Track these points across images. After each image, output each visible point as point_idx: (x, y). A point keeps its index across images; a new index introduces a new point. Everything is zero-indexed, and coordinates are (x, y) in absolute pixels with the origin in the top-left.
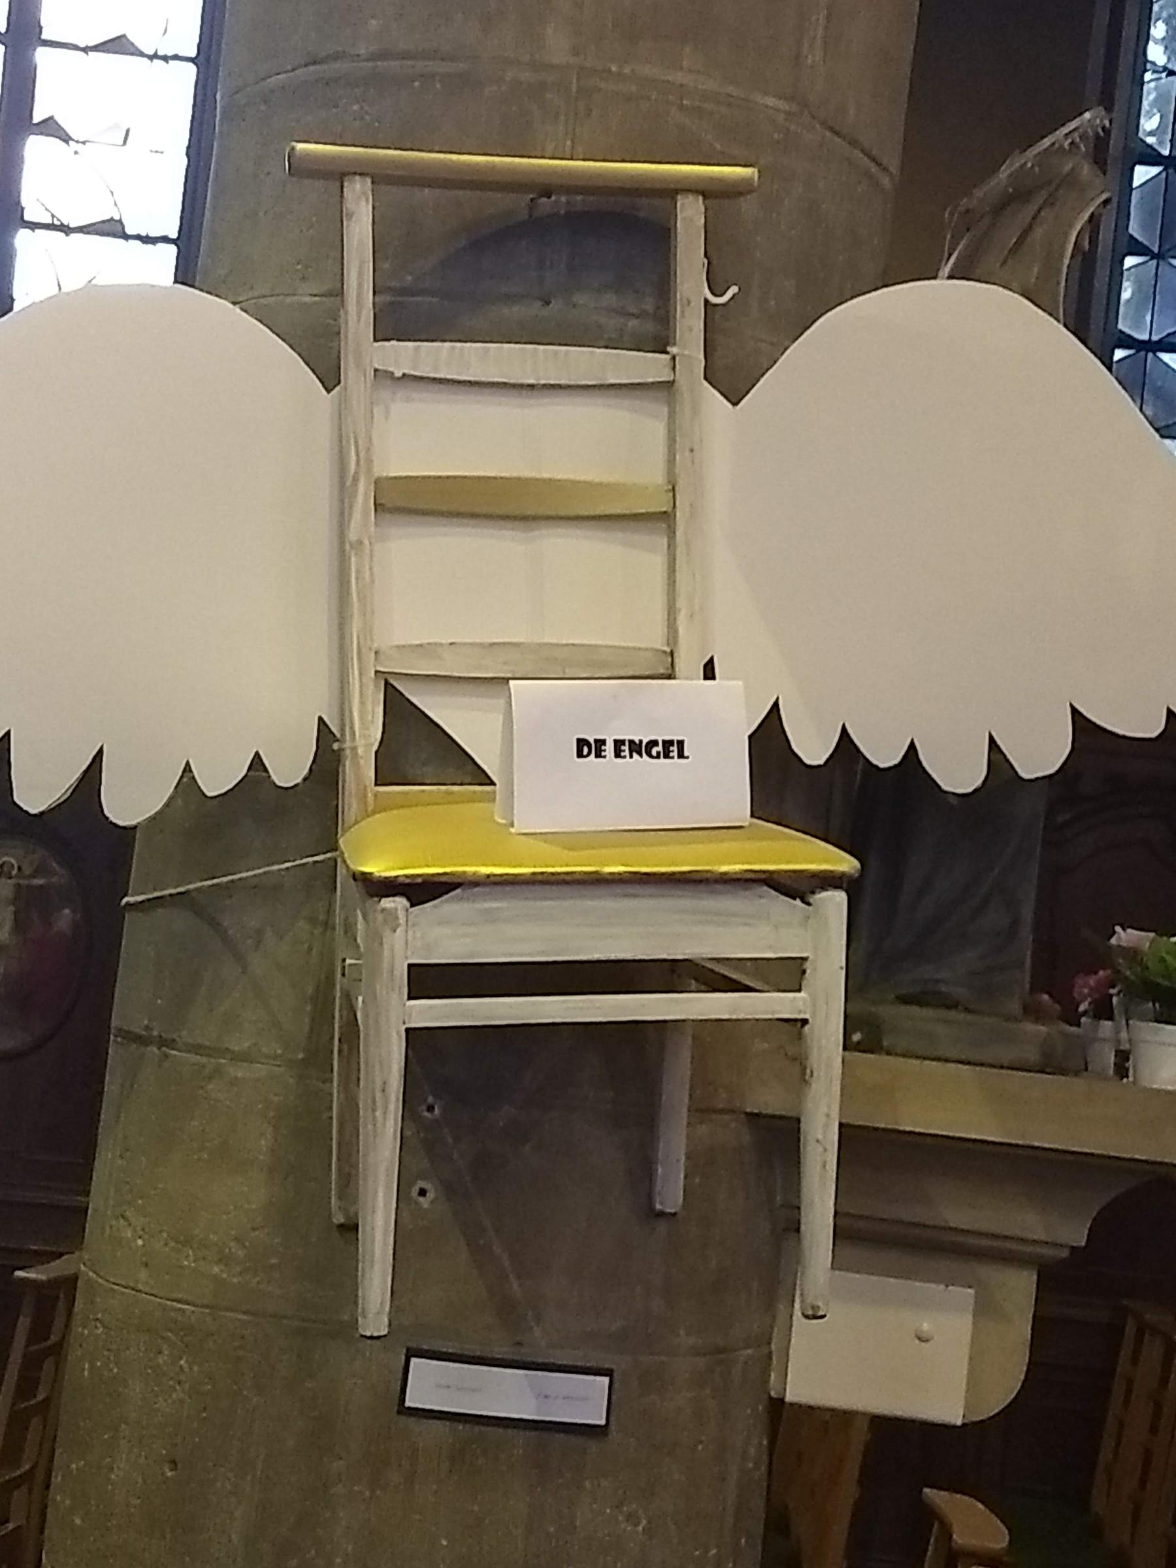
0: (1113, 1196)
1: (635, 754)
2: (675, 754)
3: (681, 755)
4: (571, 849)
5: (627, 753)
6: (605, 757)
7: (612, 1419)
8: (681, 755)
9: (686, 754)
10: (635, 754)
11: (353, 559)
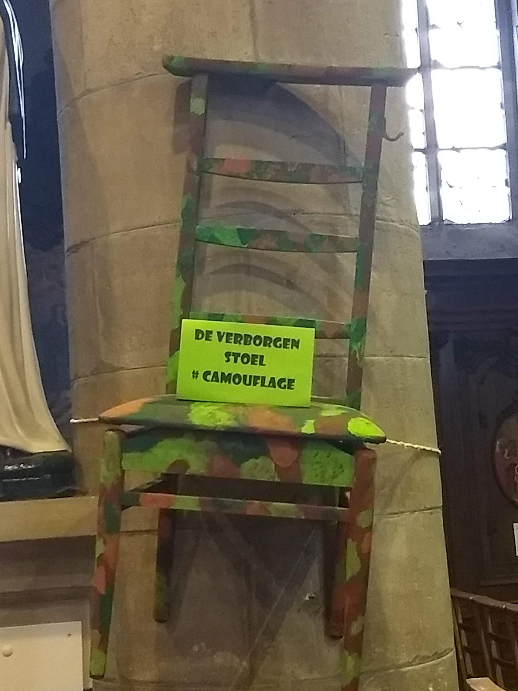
0: (50, 3)
1: (294, 347)
2: (258, 363)
3: (261, 364)
4: (176, 75)
5: (290, 346)
6: (293, 389)
7: (178, 322)
8: (261, 364)
9: (264, 363)
10: (294, 347)
11: (210, 498)
